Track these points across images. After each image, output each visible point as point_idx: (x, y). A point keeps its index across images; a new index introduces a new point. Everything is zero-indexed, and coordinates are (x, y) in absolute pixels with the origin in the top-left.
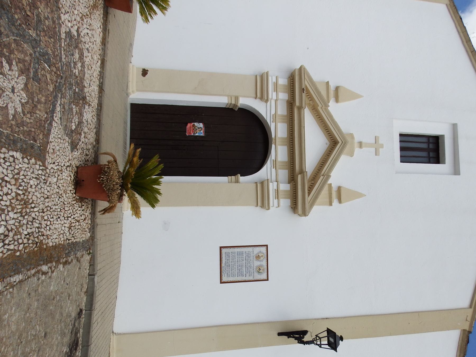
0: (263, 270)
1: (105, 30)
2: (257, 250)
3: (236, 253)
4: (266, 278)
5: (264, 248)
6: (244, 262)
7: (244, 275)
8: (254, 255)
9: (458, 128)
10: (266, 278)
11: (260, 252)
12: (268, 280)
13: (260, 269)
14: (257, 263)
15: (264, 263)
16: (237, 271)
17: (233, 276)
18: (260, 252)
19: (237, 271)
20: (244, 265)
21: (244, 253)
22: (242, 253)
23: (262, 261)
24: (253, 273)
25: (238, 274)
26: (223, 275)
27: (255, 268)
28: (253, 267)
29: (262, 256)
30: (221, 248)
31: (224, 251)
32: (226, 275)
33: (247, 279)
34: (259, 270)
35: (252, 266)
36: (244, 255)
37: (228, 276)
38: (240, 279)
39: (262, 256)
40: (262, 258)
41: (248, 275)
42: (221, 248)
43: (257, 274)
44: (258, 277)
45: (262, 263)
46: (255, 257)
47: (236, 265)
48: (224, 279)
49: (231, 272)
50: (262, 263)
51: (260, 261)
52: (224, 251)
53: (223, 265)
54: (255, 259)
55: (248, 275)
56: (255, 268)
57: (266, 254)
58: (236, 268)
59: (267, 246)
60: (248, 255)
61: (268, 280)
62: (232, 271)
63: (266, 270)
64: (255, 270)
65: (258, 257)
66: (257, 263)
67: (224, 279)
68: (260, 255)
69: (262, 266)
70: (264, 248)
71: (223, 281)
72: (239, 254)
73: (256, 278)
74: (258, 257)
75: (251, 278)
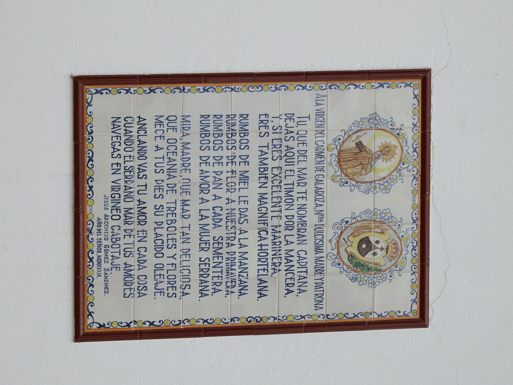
0: (393, 251)
1: (413, 219)
2: (349, 105)
3: (195, 126)
4: (405, 304)
5: (407, 94)
6: (253, 190)
7: (253, 286)
8: (329, 139)
9: (312, 71)
10: (405, 304)
11: (374, 122)
12: (421, 320)
13: (366, 246)
14: (346, 202)
15: (401, 201)
16: (196, 254)
17: (172, 286)
18: (374, 122)
19: (196, 254)
20: (253, 214)
21: (253, 124)
22: (236, 128)
23: (385, 184)
24: (319, 270)
25: (203, 274)
26: (99, 282)
27: (329, 233)
28: (319, 230)
29: (386, 151)
30: (80, 84)
31: (103, 106)
32: (117, 278)
33: (269, 309)
34: (361, 256)
35: (311, 219)
36: (255, 141)
37: (134, 287)
38: (218, 308)
39: (386, 151)
40: (383, 167)
41: (276, 283)
42: (80, 84)
43: (344, 279)
44: (348, 296)
45: (381, 201)
46: (330, 157)
47: (194, 209)
48: (106, 309)
49: (151, 260)
50: (381, 201)
51: (372, 186)
52: (103, 106)
53: (97, 209)
54: (331, 169)
55: (276, 283)
56: (329, 233)
57: (412, 136)
58: (194, 234)
59: (423, 76)
60: (285, 141)
61: (421, 320)
62: (159, 251)
63: (410, 257)
64: (328, 248)
65: (354, 159)
66: (346, 202)
67: (106, 309)
68: (373, 141)
69: (381, 221)
70: (407, 94)
71: (92, 323)
72: (211, 128)
73: (334, 308)
74: (354, 159)
75: (301, 307)
